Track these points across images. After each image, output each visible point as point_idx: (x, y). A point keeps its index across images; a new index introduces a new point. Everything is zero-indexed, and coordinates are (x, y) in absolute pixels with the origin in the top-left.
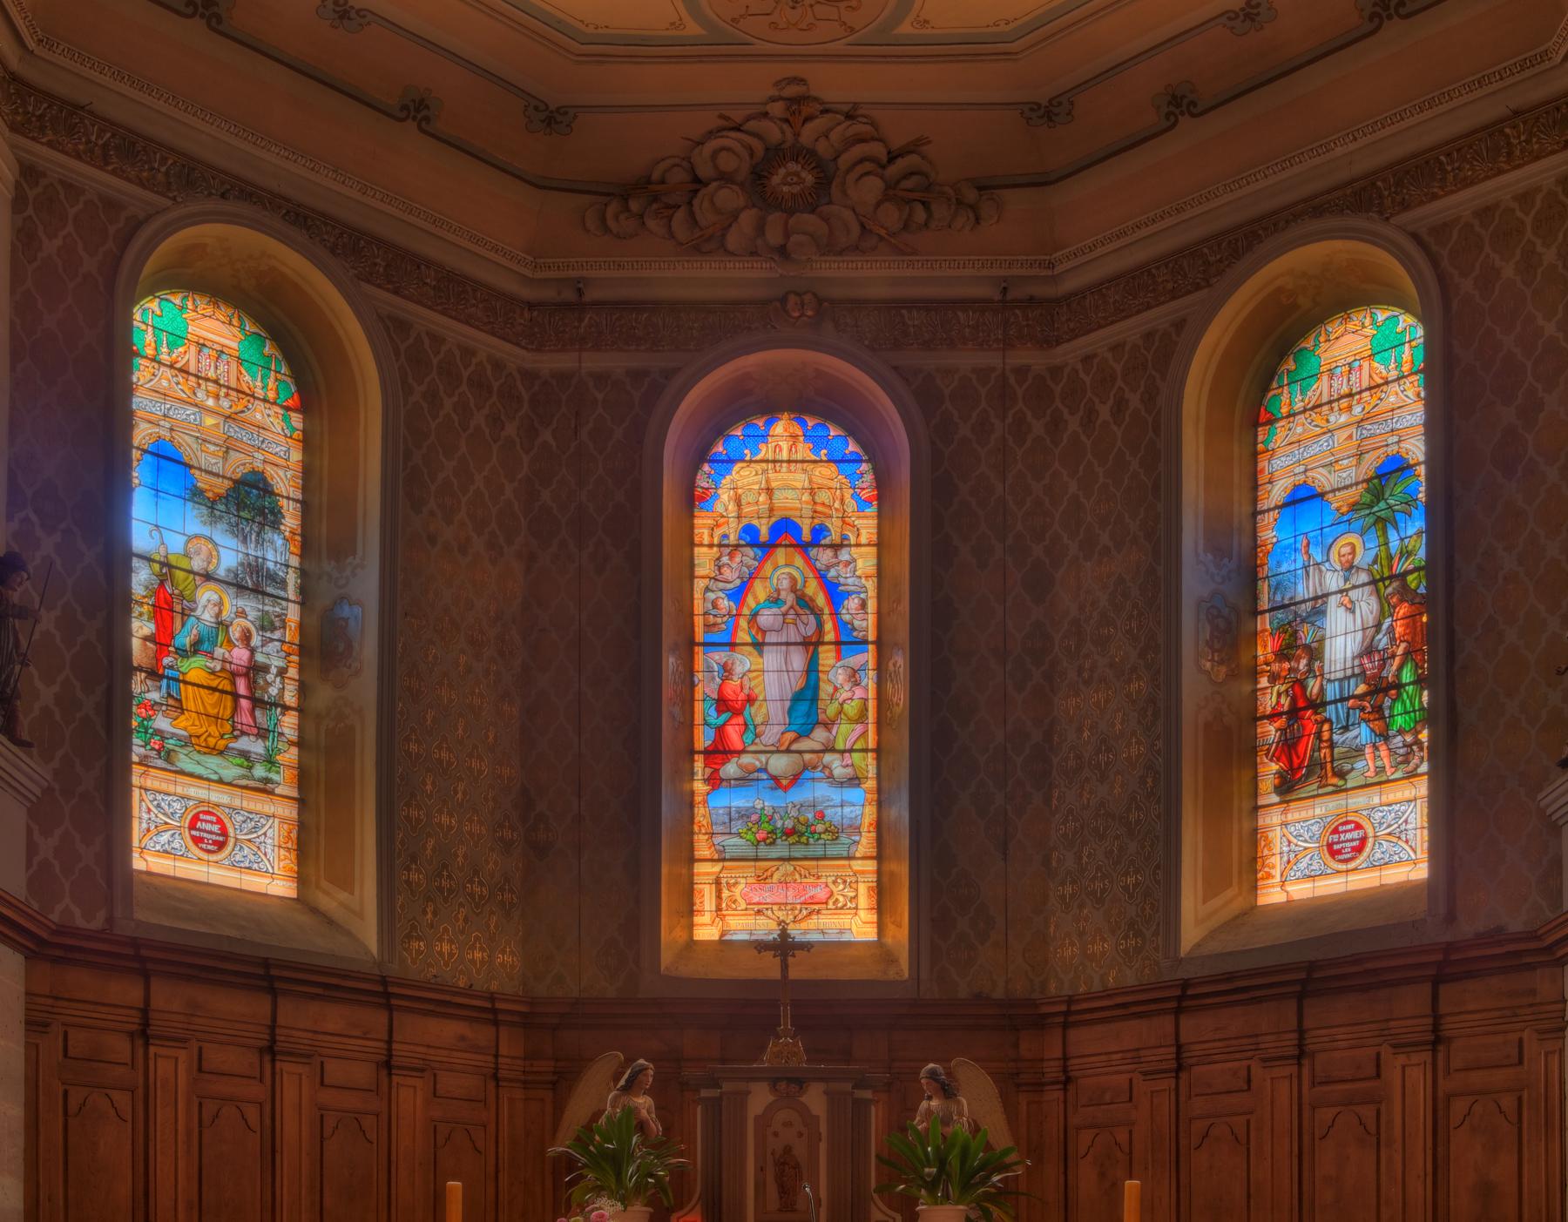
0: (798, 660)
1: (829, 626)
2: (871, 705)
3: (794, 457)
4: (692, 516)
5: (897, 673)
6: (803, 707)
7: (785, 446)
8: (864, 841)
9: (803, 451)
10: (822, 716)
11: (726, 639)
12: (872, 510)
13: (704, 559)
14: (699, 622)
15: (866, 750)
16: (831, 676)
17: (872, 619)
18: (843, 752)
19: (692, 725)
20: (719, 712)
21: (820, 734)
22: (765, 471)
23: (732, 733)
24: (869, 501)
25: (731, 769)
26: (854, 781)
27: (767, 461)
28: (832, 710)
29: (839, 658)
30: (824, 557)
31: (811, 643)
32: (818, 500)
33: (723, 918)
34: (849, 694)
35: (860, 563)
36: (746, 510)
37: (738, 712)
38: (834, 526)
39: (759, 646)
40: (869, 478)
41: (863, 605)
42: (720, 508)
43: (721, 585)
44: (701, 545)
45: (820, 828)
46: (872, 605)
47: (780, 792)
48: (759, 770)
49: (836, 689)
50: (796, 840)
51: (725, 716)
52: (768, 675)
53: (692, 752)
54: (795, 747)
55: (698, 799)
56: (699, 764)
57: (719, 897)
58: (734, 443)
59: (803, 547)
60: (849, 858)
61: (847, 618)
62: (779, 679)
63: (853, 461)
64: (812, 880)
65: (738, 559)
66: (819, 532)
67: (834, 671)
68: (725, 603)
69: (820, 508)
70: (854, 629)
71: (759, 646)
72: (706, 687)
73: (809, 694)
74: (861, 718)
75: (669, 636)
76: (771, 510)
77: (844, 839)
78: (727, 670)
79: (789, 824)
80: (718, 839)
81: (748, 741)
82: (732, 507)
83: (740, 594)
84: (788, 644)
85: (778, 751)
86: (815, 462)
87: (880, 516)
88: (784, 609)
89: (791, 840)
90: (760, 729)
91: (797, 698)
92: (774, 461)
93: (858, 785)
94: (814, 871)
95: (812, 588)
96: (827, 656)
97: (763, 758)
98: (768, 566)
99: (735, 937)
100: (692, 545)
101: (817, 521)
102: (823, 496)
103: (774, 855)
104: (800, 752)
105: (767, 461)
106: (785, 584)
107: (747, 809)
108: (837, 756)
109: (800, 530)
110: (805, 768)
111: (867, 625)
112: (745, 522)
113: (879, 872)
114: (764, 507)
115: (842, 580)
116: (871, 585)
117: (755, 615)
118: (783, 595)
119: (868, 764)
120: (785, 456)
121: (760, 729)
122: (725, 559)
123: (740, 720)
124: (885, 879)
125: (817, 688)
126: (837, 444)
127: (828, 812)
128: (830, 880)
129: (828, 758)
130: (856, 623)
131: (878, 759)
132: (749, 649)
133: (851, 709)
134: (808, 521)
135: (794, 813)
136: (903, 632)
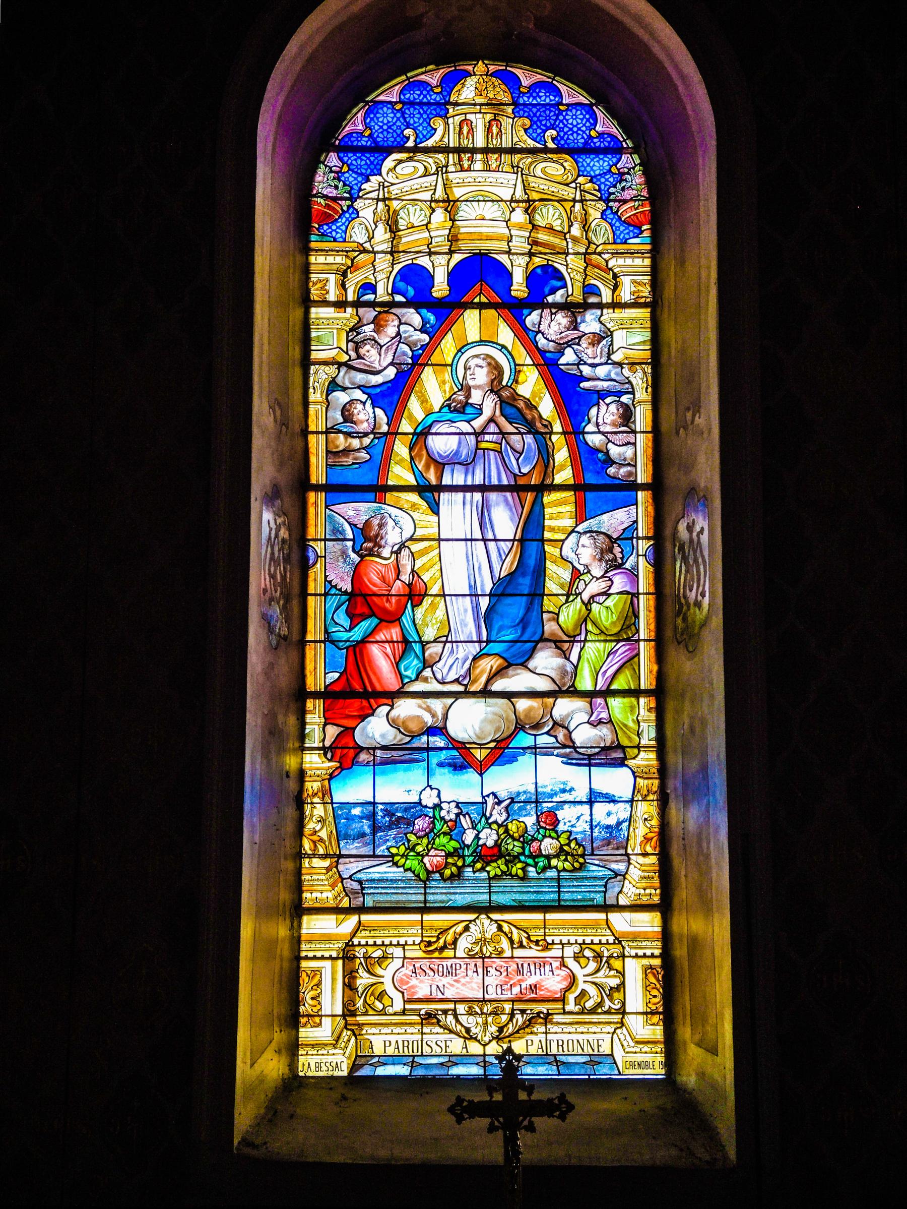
0: (505, 521)
1: (561, 455)
2: (645, 605)
3: (495, 143)
4: (306, 250)
5: (695, 545)
6: (514, 608)
7: (479, 122)
8: (635, 873)
9: (514, 131)
10: (550, 627)
11: (366, 478)
12: (641, 242)
13: (329, 331)
14: (317, 445)
15: (635, 693)
16: (567, 551)
17: (643, 442)
18: (589, 695)
19: (302, 643)
20: (355, 618)
21: (546, 660)
22: (442, 169)
23: (380, 658)
24: (635, 225)
25: (376, 729)
26: (612, 755)
27: (446, 150)
28: (569, 615)
29: (581, 516)
30: (552, 326)
31: (528, 488)
32: (539, 221)
33: (356, 1030)
34: (601, 586)
35: (620, 339)
36: (407, 239)
37: (392, 618)
38: (571, 268)
39: (430, 492)
40: (637, 180)
41: (627, 415)
42: (358, 235)
43: (360, 378)
44: (325, 303)
45: (548, 846)
46: (642, 417)
47: (471, 775)
48: (432, 731)
49: (576, 574)
50: (517, 864)
51: (365, 626)
52: (452, 550)
53: (301, 694)
54: (498, 685)
55: (312, 786)
56: (314, 718)
57: (349, 986)
58: (386, 116)
59: (514, 310)
60: (605, 908)
61: (595, 440)
62: (469, 558)
63: (605, 151)
64: (533, 952)
65: (391, 330)
66: (544, 279)
67: (572, 547)
68: (367, 415)
69: (542, 237)
70: (609, 462)
71: (430, 492)
72: (332, 569)
73: (525, 584)
74: (625, 632)
75: (263, 470)
76: (453, 238)
77: (594, 869)
78: (368, 539)
79: (489, 837)
80: (349, 868)
81: (411, 673)
82: (381, 234)
83: (393, 395)
84: (483, 488)
85: (467, 694)
86: (532, 151)
87: (655, 253)
88: (478, 423)
89: (492, 869)
90: (434, 650)
91: (503, 590)
92: (459, 150)
93: (621, 763)
94: (537, 934)
95: (530, 383)
96: (559, 511)
97: (437, 705)
98: (448, 346)
99: (381, 1071)
100: (307, 302)
101: (538, 261)
102: (549, 215)
103: (460, 900)
104: (509, 696)
105: (446, 150)
106: (481, 377)
107: (408, 807)
108: (580, 704)
109: (508, 276)
110: (520, 727)
111: (633, 455)
112: (404, 261)
113: (666, 936)
114: (440, 236)
115: (586, 370)
116: (639, 380)
117: (422, 434)
118: (476, 397)
119: (635, 718)
120: (480, 142)
121: (434, 650)
122: (368, 329)
123: (394, 633)
124: (680, 952)
125: (540, 572)
126: (576, 119)
127: (566, 815)
128: (569, 951)
129: (563, 707)
130: (614, 451)
131: (660, 712)
132: (414, 497)
133: (607, 614)
134: (522, 261)
135: (498, 816)
136: (707, 468)
